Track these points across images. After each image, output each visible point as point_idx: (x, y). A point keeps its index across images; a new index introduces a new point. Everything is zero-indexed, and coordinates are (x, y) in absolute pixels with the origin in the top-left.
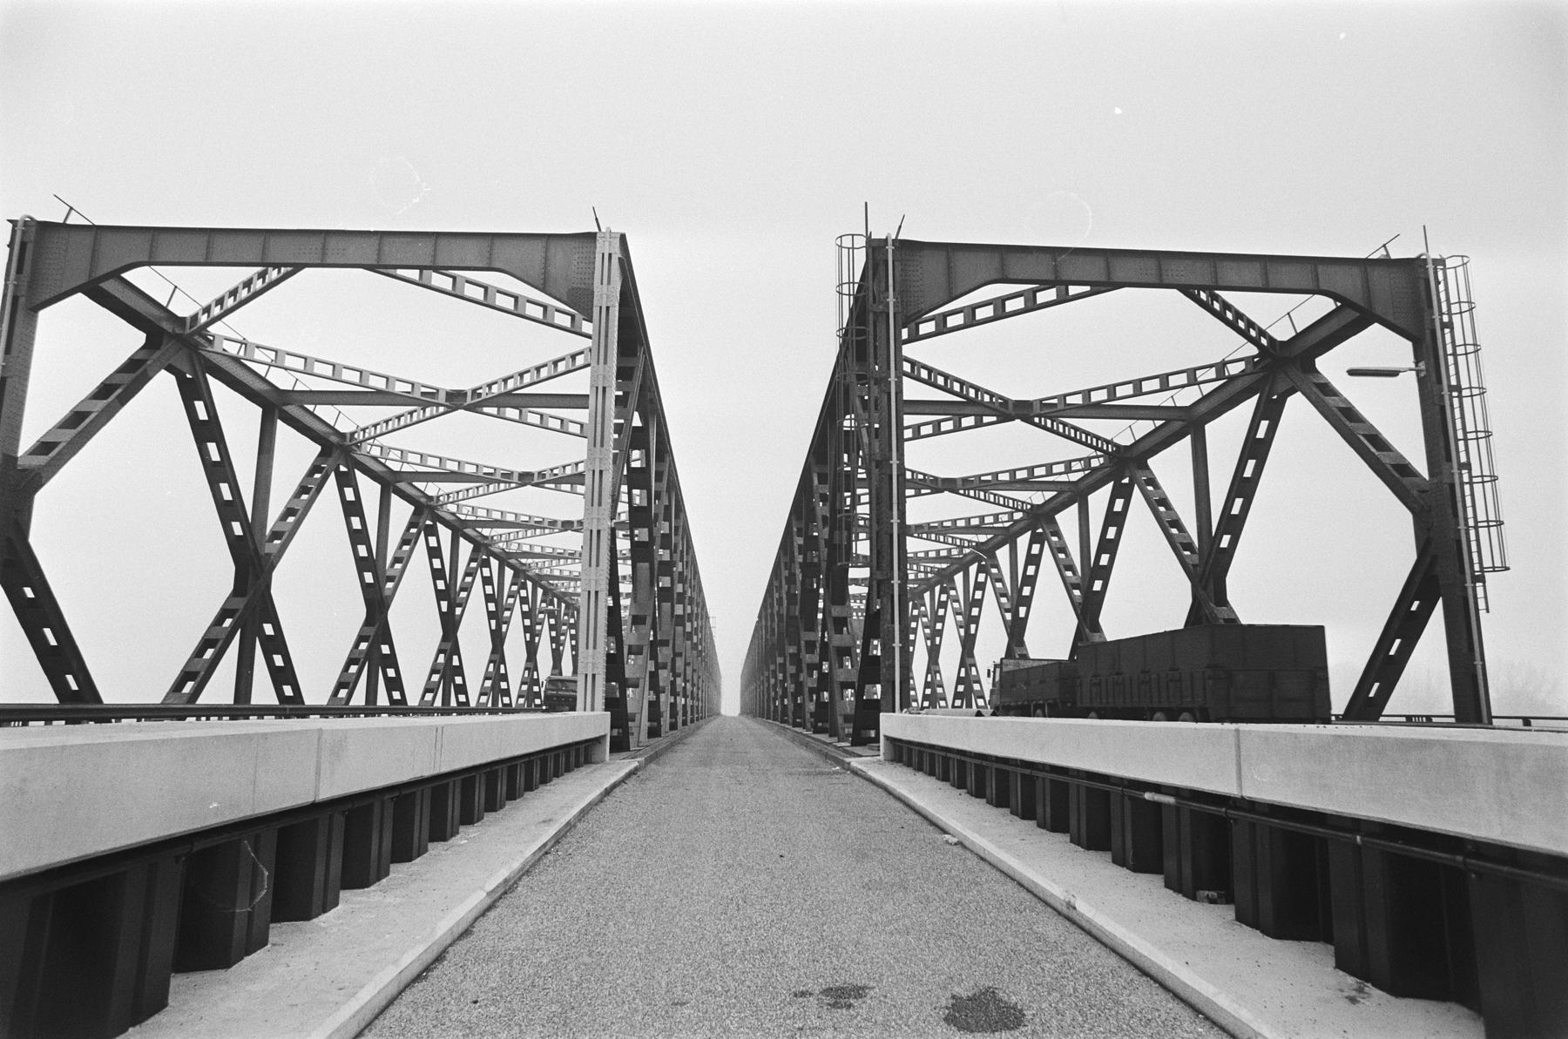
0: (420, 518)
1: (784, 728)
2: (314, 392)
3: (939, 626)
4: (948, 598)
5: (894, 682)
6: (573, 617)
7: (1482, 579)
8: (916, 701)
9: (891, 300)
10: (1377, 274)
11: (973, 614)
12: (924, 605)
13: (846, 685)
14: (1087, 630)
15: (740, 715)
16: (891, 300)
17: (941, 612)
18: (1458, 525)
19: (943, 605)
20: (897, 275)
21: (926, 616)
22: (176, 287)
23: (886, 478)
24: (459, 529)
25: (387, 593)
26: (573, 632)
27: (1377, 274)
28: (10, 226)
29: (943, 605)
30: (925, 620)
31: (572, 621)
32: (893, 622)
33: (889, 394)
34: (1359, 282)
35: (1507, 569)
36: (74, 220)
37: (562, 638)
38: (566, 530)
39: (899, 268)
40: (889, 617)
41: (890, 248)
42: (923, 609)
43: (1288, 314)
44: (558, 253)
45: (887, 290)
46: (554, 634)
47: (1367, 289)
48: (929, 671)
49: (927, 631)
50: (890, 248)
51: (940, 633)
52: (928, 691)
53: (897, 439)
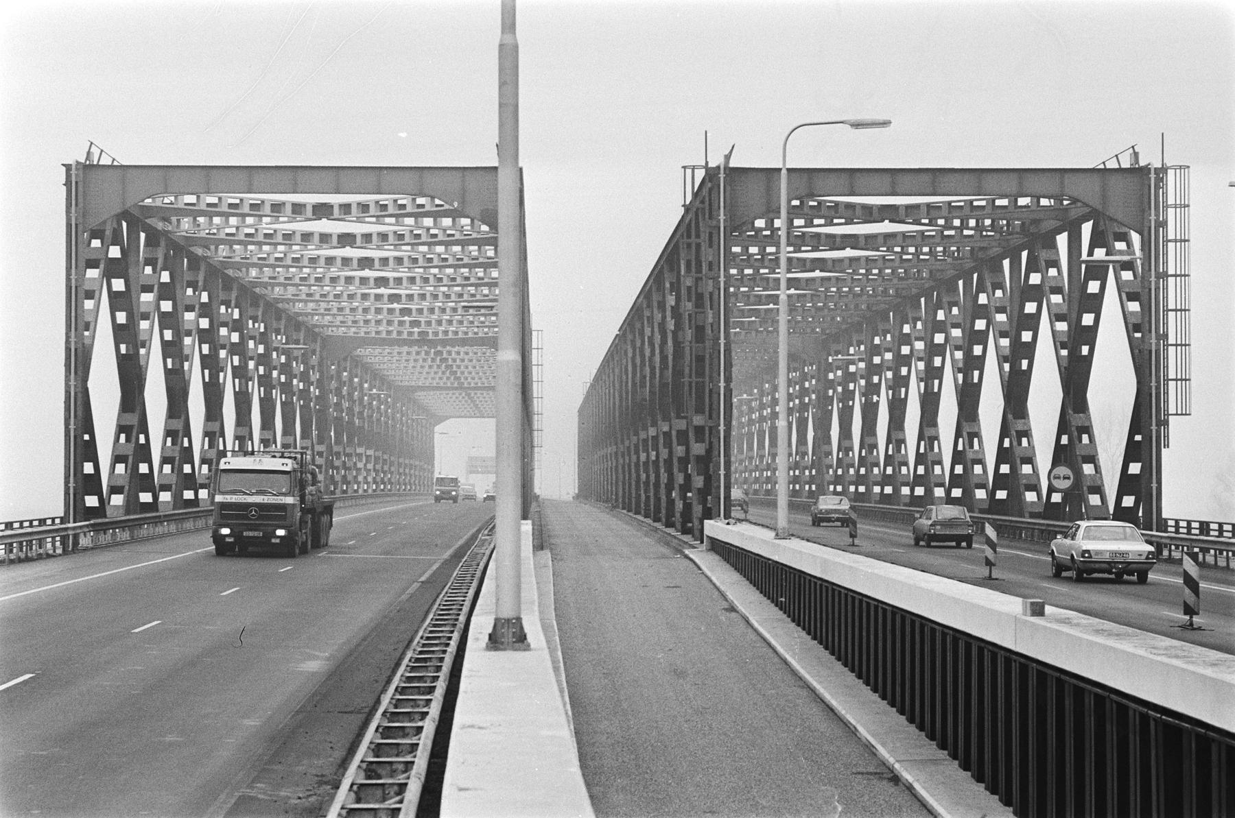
0: (258, 310)
1: (656, 529)
2: (124, 166)
3: (1088, 319)
4: (947, 339)
5: (719, 499)
6: (116, 240)
7: (1166, 423)
8: (1035, 487)
9: (722, 217)
10: (1115, 183)
11: (1084, 323)
12: (1055, 264)
13: (806, 468)
14: (1070, 412)
15: (577, 497)
16: (722, 217)
17: (1093, 287)
18: (1151, 382)
19: (1097, 271)
20: (727, 199)
21: (1057, 290)
22: (102, 151)
23: (716, 352)
24: (138, 220)
25: (87, 342)
26: (118, 285)
27: (1115, 183)
28: (64, 168)
29: (1097, 271)
30: (1056, 299)
31: (115, 252)
32: (719, 456)
33: (719, 289)
34: (1097, 189)
35: (1190, 414)
36: (115, 163)
37: (144, 325)
38: (344, 247)
39: (728, 188)
40: (717, 453)
41: (722, 176)
42: (1053, 272)
43: (1116, 156)
44: (472, 183)
45: (719, 208)
46: (121, 317)
47: (1104, 197)
48: (1063, 427)
49: (1062, 326)
50: (722, 176)
51: (1089, 335)
52: (1005, 469)
53: (725, 326)
